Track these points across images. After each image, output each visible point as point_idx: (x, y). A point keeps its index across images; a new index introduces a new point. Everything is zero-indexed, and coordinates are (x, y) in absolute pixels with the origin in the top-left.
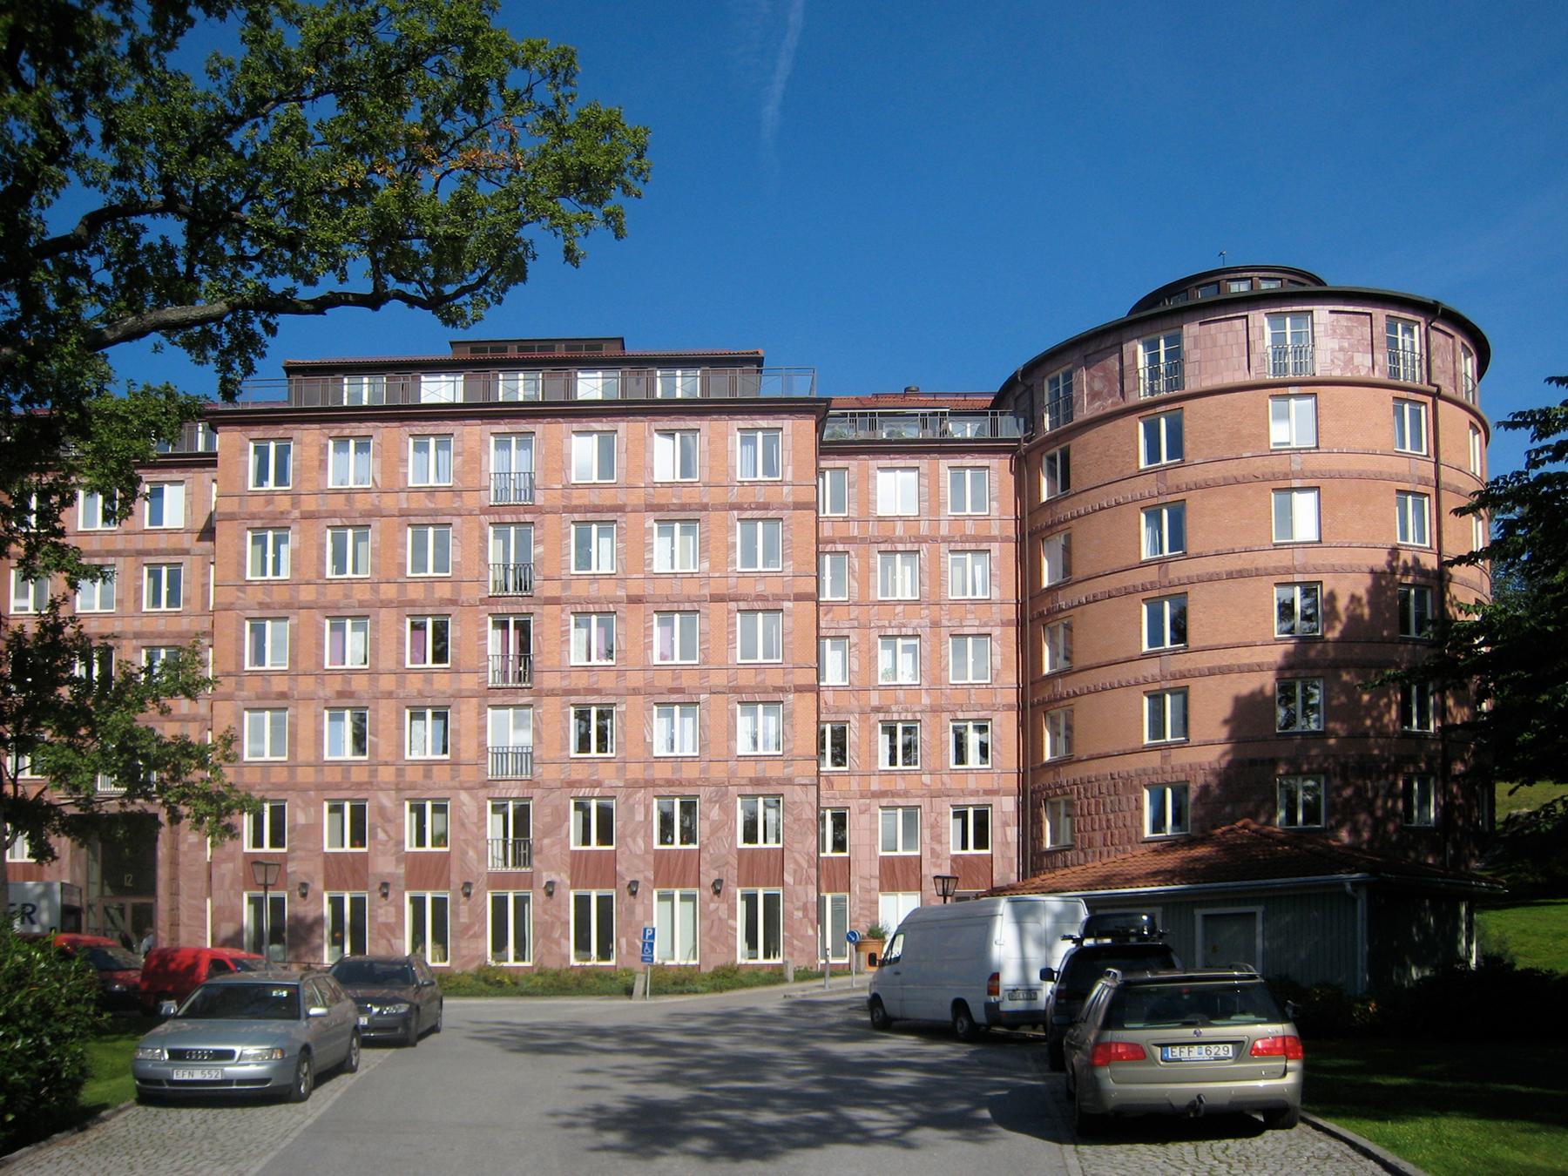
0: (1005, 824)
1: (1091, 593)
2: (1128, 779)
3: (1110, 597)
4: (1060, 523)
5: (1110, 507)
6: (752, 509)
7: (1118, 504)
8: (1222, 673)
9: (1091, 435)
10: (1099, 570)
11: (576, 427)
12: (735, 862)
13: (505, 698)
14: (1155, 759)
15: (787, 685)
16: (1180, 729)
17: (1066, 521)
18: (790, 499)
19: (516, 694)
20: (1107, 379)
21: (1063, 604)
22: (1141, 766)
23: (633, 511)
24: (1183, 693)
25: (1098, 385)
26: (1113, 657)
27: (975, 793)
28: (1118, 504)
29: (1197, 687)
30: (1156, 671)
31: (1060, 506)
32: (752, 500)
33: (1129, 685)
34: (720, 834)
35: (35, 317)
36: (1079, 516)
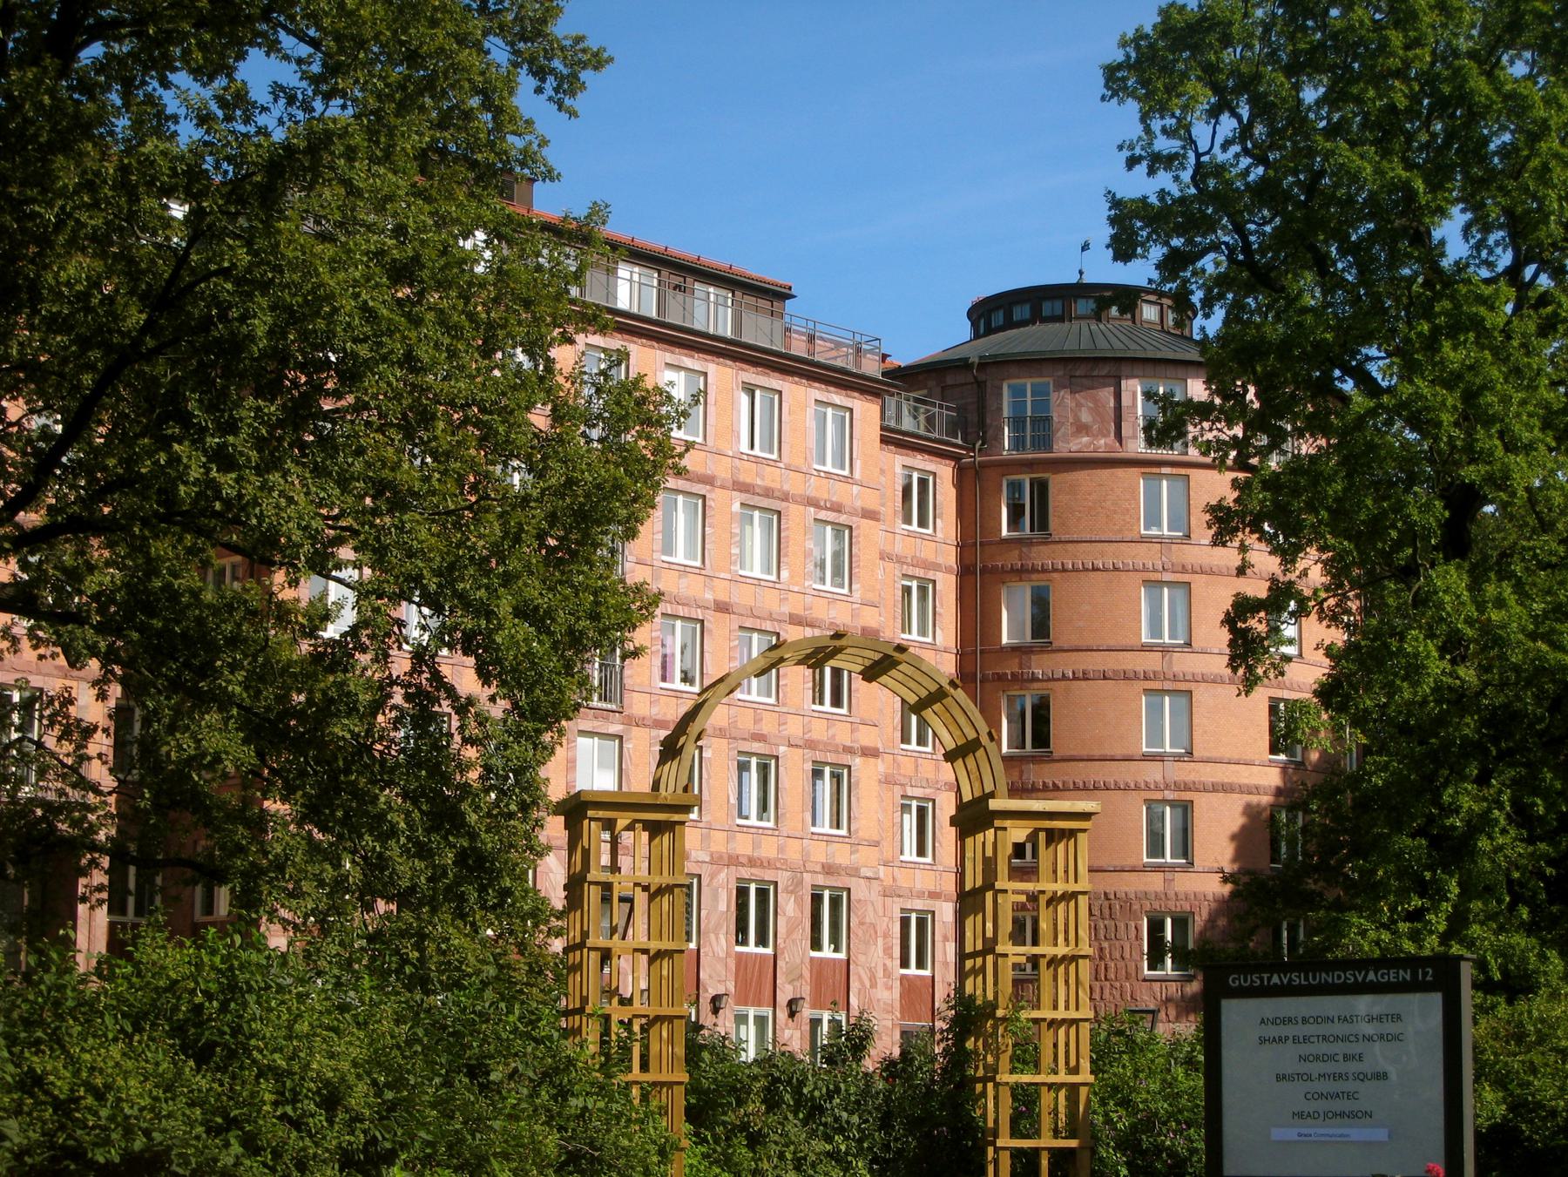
0: (946, 939)
1: (1081, 667)
2: (1127, 903)
3: (1105, 678)
4: (1034, 570)
5: (1106, 570)
6: (827, 509)
7: (1116, 569)
8: (1225, 791)
9: (1082, 477)
10: (1094, 645)
11: (669, 357)
12: (807, 974)
13: (596, 723)
14: (1155, 882)
15: (856, 745)
16: (1180, 851)
17: (1044, 571)
18: (859, 504)
19: (607, 718)
20: (1097, 410)
21: (1039, 673)
22: (1142, 888)
23: (722, 487)
24: (1185, 810)
25: (1085, 417)
26: (1109, 752)
27: (920, 895)
28: (1116, 569)
29: (1202, 803)
30: (1159, 778)
31: (1035, 549)
32: (826, 496)
33: (1127, 788)
34: (794, 936)
35: (1256, 405)
36: (1064, 570)
